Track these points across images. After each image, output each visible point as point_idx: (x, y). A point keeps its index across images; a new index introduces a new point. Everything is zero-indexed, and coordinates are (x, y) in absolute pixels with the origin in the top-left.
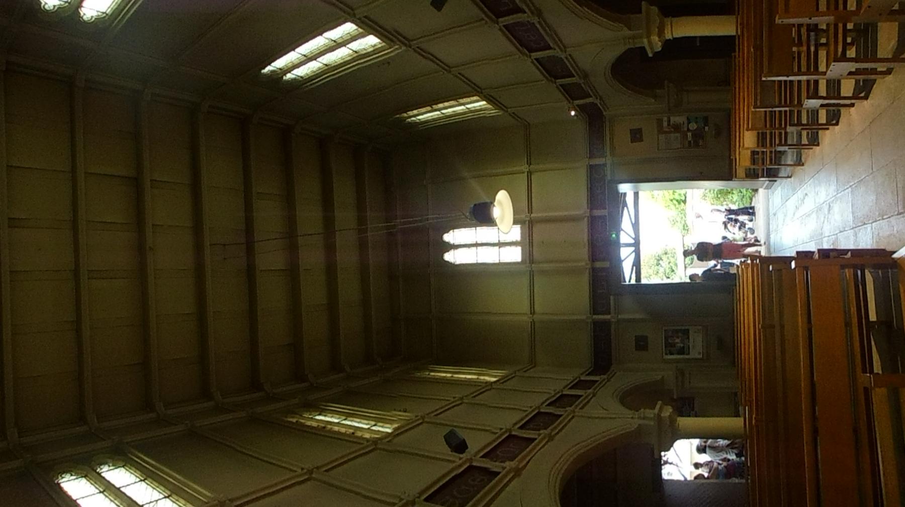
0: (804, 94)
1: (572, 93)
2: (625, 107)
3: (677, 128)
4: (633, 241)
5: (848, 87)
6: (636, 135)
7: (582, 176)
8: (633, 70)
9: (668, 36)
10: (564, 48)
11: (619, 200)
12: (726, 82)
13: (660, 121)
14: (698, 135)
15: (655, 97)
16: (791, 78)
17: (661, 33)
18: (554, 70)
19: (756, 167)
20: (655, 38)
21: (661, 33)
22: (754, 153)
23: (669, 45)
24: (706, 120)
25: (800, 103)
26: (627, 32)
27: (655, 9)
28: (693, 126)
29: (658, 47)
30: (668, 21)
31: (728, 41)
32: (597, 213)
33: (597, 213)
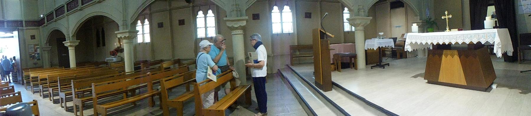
0: (67, 92)
1: (50, 17)
2: (43, 34)
3: (36, 51)
4: (313, 61)
5: (70, 104)
6: (33, 37)
7: (19, 18)
8: (57, 38)
9: (69, 48)
10: (67, 15)
11: (11, 31)
12: (52, 66)
13: (38, 45)
14: (34, 57)
15: (46, 43)
16: (73, 89)
17: (70, 46)
18: (59, 11)
19: (39, 80)
20: (69, 44)
21: (70, 46)
22: (37, 77)
23: (66, 49)
24: (39, 59)
25: (50, 87)
26: (71, 36)
27: (77, 44)
28: (36, 55)
29: (66, 45)
30: (74, 48)
31: (67, 65)
32: (5, 24)
33: (5, 24)
